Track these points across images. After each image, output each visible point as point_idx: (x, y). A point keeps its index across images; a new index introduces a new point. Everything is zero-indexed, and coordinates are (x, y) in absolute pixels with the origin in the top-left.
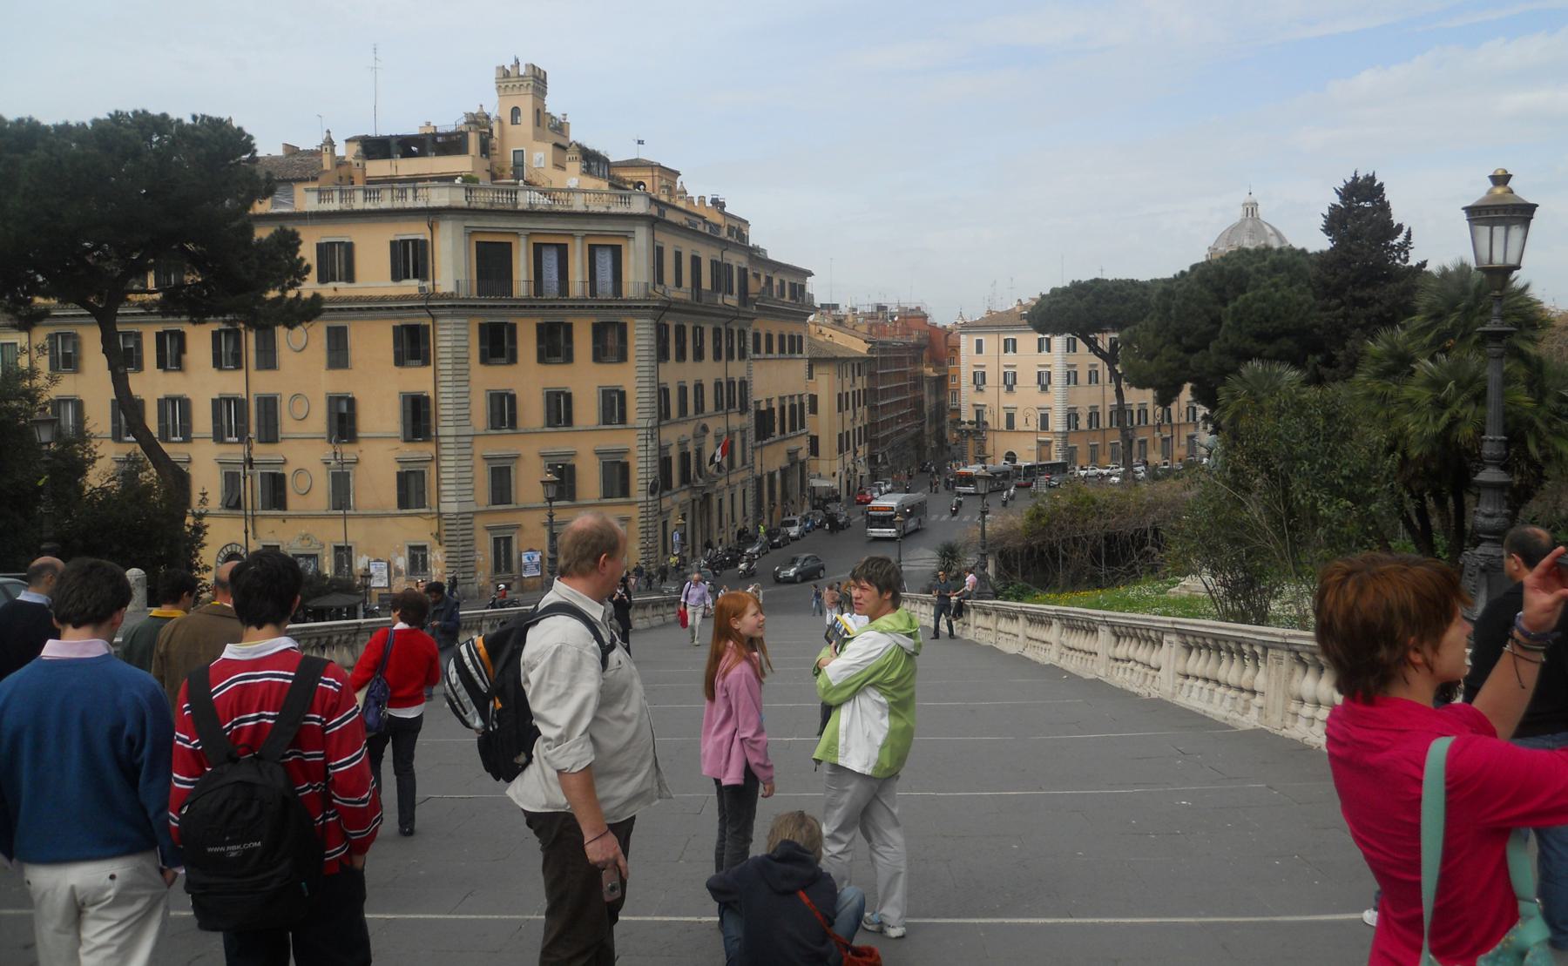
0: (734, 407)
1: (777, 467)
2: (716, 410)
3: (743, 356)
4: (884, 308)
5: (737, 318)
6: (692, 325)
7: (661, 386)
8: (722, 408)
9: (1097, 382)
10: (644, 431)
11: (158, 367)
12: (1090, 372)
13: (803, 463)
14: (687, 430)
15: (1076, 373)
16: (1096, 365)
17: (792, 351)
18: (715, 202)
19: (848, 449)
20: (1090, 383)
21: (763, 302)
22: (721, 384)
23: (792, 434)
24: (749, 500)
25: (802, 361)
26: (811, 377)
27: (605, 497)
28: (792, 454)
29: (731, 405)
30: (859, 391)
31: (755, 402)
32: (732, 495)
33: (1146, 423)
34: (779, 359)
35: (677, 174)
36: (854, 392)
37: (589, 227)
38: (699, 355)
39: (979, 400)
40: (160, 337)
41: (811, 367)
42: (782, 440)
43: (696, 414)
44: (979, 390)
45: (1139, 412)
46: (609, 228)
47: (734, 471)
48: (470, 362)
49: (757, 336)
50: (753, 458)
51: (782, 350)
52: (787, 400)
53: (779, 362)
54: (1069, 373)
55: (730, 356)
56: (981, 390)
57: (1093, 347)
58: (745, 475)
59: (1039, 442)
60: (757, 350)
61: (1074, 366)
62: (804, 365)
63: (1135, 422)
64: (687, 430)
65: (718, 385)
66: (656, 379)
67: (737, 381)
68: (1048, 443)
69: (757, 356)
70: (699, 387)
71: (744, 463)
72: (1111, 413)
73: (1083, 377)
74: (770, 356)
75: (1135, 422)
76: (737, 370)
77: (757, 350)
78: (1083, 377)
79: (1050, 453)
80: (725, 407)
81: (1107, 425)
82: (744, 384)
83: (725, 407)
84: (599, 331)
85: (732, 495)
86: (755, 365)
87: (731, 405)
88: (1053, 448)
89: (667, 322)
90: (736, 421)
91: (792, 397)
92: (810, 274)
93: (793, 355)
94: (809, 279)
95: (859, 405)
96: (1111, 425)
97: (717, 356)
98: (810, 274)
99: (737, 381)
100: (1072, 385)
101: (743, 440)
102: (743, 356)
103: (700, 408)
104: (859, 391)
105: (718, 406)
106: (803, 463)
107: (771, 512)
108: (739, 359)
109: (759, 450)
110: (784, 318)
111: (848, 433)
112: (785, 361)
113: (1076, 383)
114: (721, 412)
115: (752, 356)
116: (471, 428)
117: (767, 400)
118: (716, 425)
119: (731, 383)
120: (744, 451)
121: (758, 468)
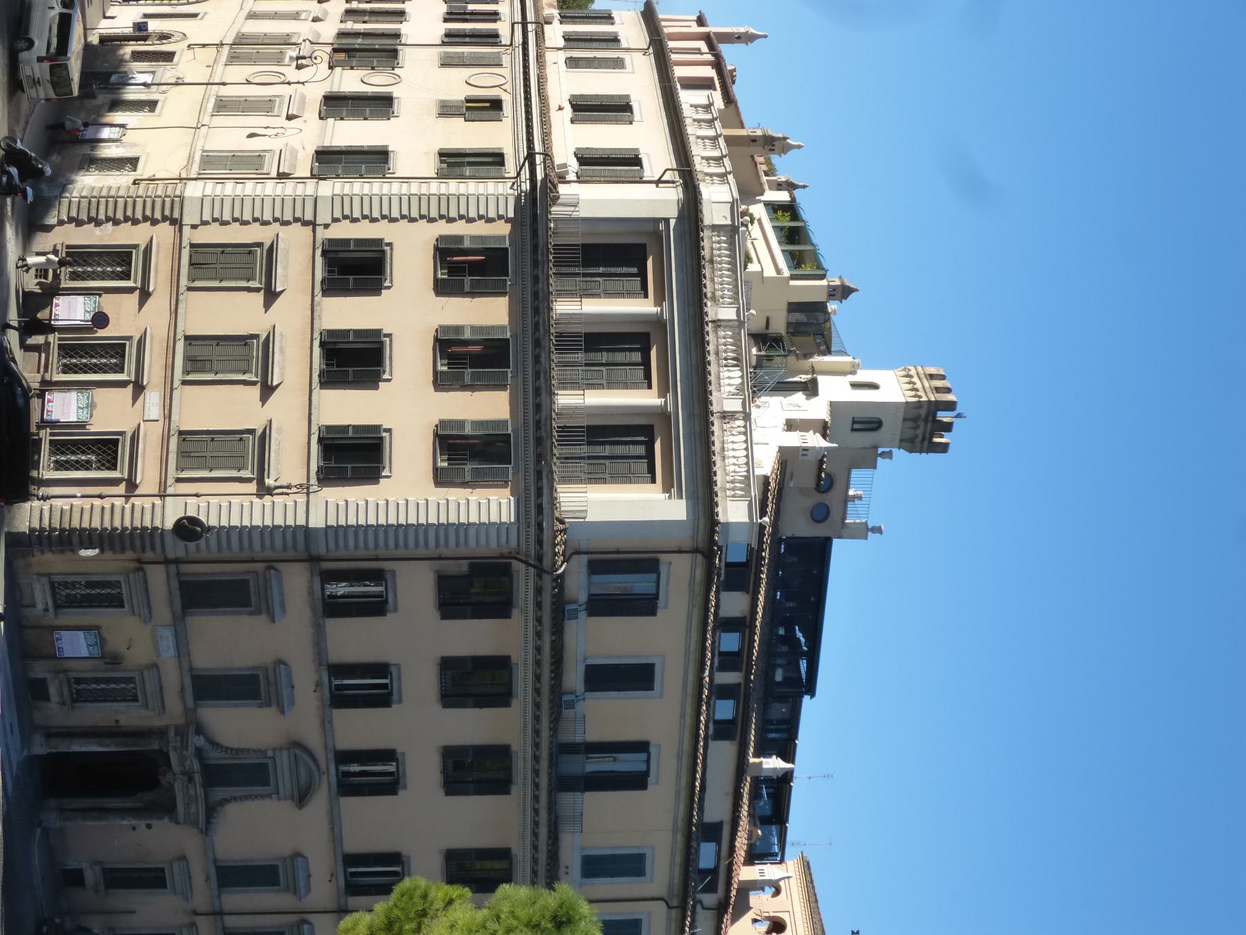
84: (499, 665)
116: (329, 221)
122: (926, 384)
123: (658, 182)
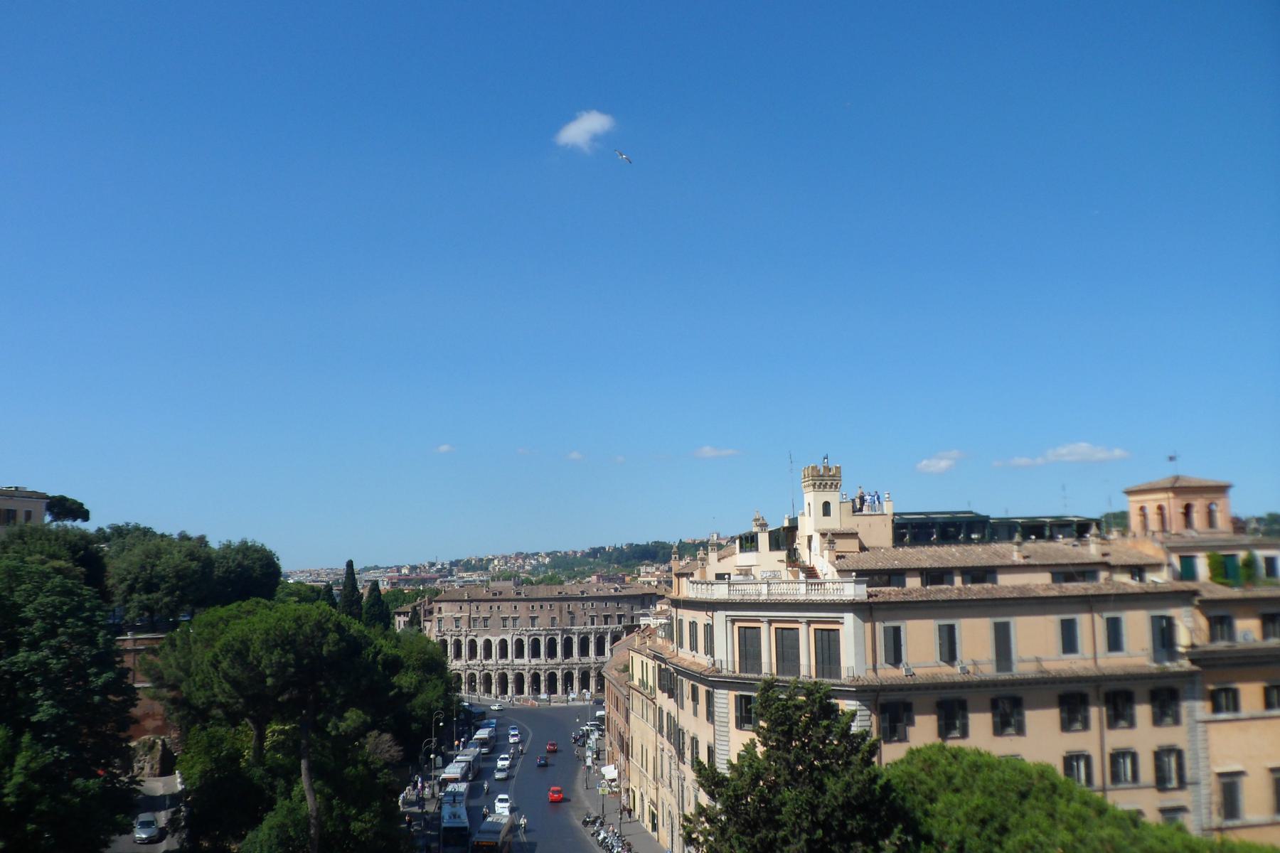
48: (729, 725)
122: (807, 479)
123: (712, 618)
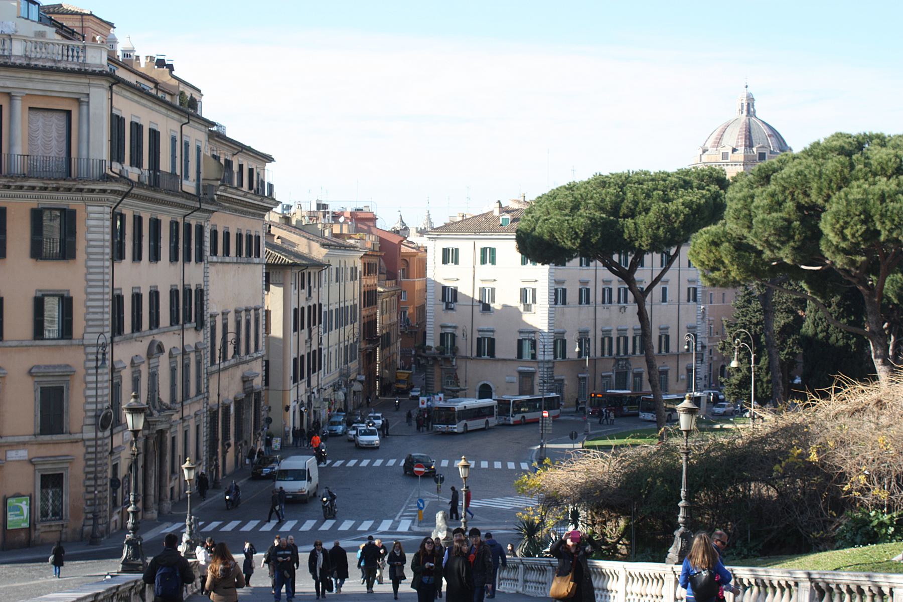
0: (190, 321)
1: (231, 398)
2: (171, 325)
3: (200, 258)
4: (325, 206)
5: (199, 209)
6: (170, 219)
7: (116, 292)
8: (177, 323)
9: (588, 302)
10: (94, 350)
11: (564, 265)
12: (580, 290)
13: (258, 394)
14: (140, 348)
15: (564, 290)
16: (610, 282)
17: (249, 254)
18: (161, 63)
19: (302, 377)
20: (580, 303)
21: (225, 191)
22: (177, 291)
23: (248, 358)
24: (203, 439)
25: (260, 267)
26: (268, 289)
27: (43, 432)
28: (246, 380)
29: (187, 319)
30: (315, 305)
31: (211, 316)
32: (186, 432)
33: (667, 350)
34: (237, 263)
35: (111, 25)
36: (309, 307)
37: (30, 85)
38: (155, 256)
39: (449, 319)
40: (37, 216)
41: (267, 276)
42: (237, 365)
43: (150, 329)
44: (448, 308)
45: (618, 339)
46: (57, 88)
47: (189, 401)
49: (214, 233)
50: (208, 387)
51: (239, 253)
52: (243, 314)
53: (236, 266)
54: (556, 290)
55: (187, 259)
56: (452, 309)
57: (609, 265)
58: (197, 407)
59: (520, 373)
60: (214, 252)
61: (563, 282)
62: (259, 272)
63: (630, 351)
64: (140, 348)
65: (174, 293)
66: (109, 284)
67: (193, 288)
68: (531, 375)
69: (215, 259)
70: (155, 295)
71: (199, 392)
72: (634, 338)
73: (572, 296)
74: (227, 259)
75: (630, 351)
76: (194, 274)
77: (214, 252)
78: (572, 296)
79: (532, 386)
80: (181, 322)
81: (599, 354)
82: (201, 293)
83: (181, 322)
85: (186, 432)
86: (212, 270)
87: (187, 319)
88: (537, 380)
89: (124, 212)
90: (192, 338)
91: (247, 310)
92: (269, 159)
93: (250, 260)
94: (268, 166)
95: (314, 324)
96: (603, 354)
97: (174, 258)
98: (269, 159)
99: (193, 288)
100: (559, 305)
101: (198, 363)
102: (200, 258)
103: (155, 322)
104: (315, 305)
105: (174, 320)
106: (258, 394)
107: (225, 452)
108: (196, 262)
109: (216, 376)
110: (242, 212)
111: (303, 357)
112: (242, 266)
113: (564, 303)
114: (176, 327)
115: (210, 259)
117: (223, 314)
118: (170, 341)
119: (187, 291)
120: (198, 377)
121: (213, 399)
